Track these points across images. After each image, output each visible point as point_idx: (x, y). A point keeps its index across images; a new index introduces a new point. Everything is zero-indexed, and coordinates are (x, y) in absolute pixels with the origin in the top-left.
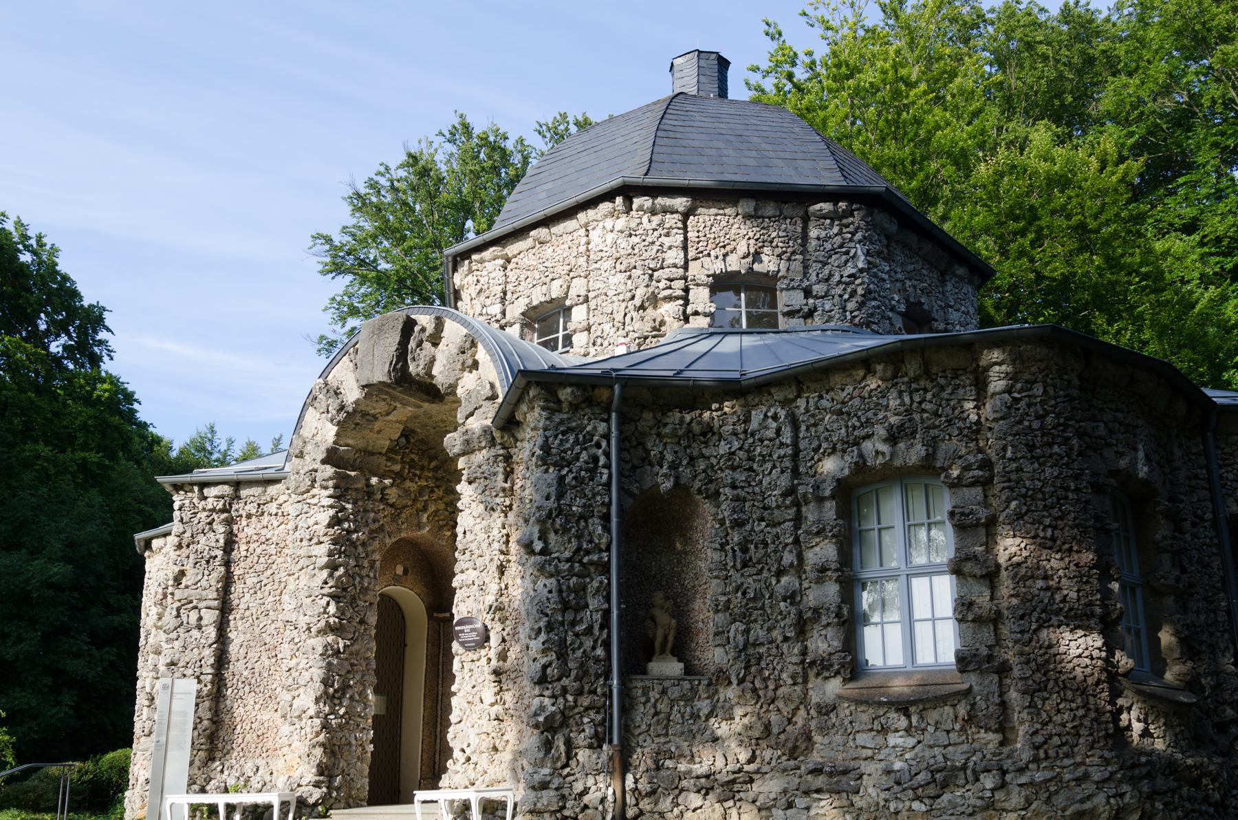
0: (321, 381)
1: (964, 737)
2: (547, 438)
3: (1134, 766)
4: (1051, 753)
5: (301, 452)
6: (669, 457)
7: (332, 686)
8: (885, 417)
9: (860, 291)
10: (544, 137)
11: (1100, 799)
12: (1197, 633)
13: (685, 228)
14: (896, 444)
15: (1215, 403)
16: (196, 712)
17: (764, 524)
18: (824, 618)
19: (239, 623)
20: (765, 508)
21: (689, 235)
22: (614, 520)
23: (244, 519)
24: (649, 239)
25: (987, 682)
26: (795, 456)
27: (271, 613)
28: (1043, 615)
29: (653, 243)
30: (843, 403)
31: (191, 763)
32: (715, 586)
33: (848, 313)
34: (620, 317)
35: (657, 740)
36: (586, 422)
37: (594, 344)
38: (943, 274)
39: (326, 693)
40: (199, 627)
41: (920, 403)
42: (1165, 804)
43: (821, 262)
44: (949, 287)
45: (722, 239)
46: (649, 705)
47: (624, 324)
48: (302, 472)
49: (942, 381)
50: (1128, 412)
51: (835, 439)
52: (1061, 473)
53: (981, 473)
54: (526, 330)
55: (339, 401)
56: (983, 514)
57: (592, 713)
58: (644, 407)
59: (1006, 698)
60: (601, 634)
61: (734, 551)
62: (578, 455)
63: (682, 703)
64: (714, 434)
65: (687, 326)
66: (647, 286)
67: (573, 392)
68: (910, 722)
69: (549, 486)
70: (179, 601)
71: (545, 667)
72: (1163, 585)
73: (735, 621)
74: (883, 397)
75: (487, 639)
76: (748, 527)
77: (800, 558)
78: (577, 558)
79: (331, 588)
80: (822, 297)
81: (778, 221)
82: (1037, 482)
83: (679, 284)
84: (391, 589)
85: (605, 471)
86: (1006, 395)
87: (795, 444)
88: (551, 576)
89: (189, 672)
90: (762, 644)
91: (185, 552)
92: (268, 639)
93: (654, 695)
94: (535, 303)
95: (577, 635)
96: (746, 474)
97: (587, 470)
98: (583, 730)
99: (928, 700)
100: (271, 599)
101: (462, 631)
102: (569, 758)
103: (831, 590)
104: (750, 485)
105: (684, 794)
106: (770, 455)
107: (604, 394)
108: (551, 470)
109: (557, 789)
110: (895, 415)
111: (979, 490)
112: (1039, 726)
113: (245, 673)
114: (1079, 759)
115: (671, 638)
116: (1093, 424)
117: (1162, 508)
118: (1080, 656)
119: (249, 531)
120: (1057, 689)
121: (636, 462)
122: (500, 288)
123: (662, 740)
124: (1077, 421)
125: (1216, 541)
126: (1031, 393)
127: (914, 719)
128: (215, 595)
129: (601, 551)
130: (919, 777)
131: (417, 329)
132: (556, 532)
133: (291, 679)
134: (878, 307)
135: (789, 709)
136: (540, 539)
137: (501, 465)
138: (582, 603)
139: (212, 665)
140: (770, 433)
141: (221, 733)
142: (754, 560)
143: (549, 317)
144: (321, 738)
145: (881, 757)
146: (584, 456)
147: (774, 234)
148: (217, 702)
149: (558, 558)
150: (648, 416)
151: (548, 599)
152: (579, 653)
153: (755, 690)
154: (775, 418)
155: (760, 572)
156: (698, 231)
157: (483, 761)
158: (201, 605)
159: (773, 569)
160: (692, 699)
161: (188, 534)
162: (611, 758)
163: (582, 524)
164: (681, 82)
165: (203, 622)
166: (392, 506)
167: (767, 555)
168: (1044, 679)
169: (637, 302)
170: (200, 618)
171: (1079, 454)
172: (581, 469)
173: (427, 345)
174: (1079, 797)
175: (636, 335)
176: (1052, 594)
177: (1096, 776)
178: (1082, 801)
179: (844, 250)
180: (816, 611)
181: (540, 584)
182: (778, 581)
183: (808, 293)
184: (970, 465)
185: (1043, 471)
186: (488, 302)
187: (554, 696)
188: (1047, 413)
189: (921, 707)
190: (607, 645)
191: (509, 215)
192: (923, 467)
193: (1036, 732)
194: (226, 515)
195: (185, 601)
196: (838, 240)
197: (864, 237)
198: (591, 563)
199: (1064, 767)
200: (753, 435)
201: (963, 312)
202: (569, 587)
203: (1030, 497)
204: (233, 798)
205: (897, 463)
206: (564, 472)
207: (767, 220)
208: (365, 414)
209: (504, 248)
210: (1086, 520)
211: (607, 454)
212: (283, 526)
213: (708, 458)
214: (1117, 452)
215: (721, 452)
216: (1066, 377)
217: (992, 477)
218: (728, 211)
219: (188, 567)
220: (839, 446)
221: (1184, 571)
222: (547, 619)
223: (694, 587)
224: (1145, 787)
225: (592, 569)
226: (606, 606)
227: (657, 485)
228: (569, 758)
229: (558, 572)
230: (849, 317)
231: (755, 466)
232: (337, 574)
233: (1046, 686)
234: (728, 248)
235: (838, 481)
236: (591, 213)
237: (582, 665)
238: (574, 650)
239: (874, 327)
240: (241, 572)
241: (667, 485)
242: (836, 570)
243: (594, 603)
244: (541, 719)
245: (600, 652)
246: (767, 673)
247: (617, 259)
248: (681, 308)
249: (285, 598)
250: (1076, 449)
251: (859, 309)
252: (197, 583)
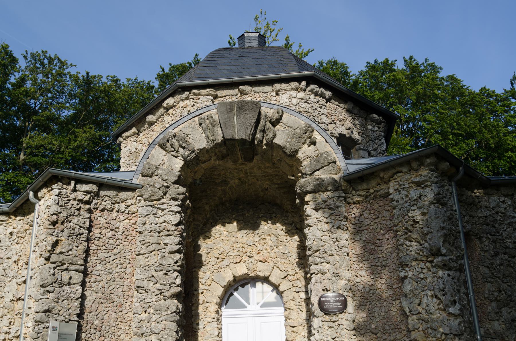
10: (26, 59)
19: (93, 285)
70: (54, 263)
79: (178, 266)
92: (116, 299)
113: (96, 322)
195: (60, 264)
212: (127, 221)
218: (341, 105)
236: (284, 86)
240: (95, 248)
252: (68, 252)
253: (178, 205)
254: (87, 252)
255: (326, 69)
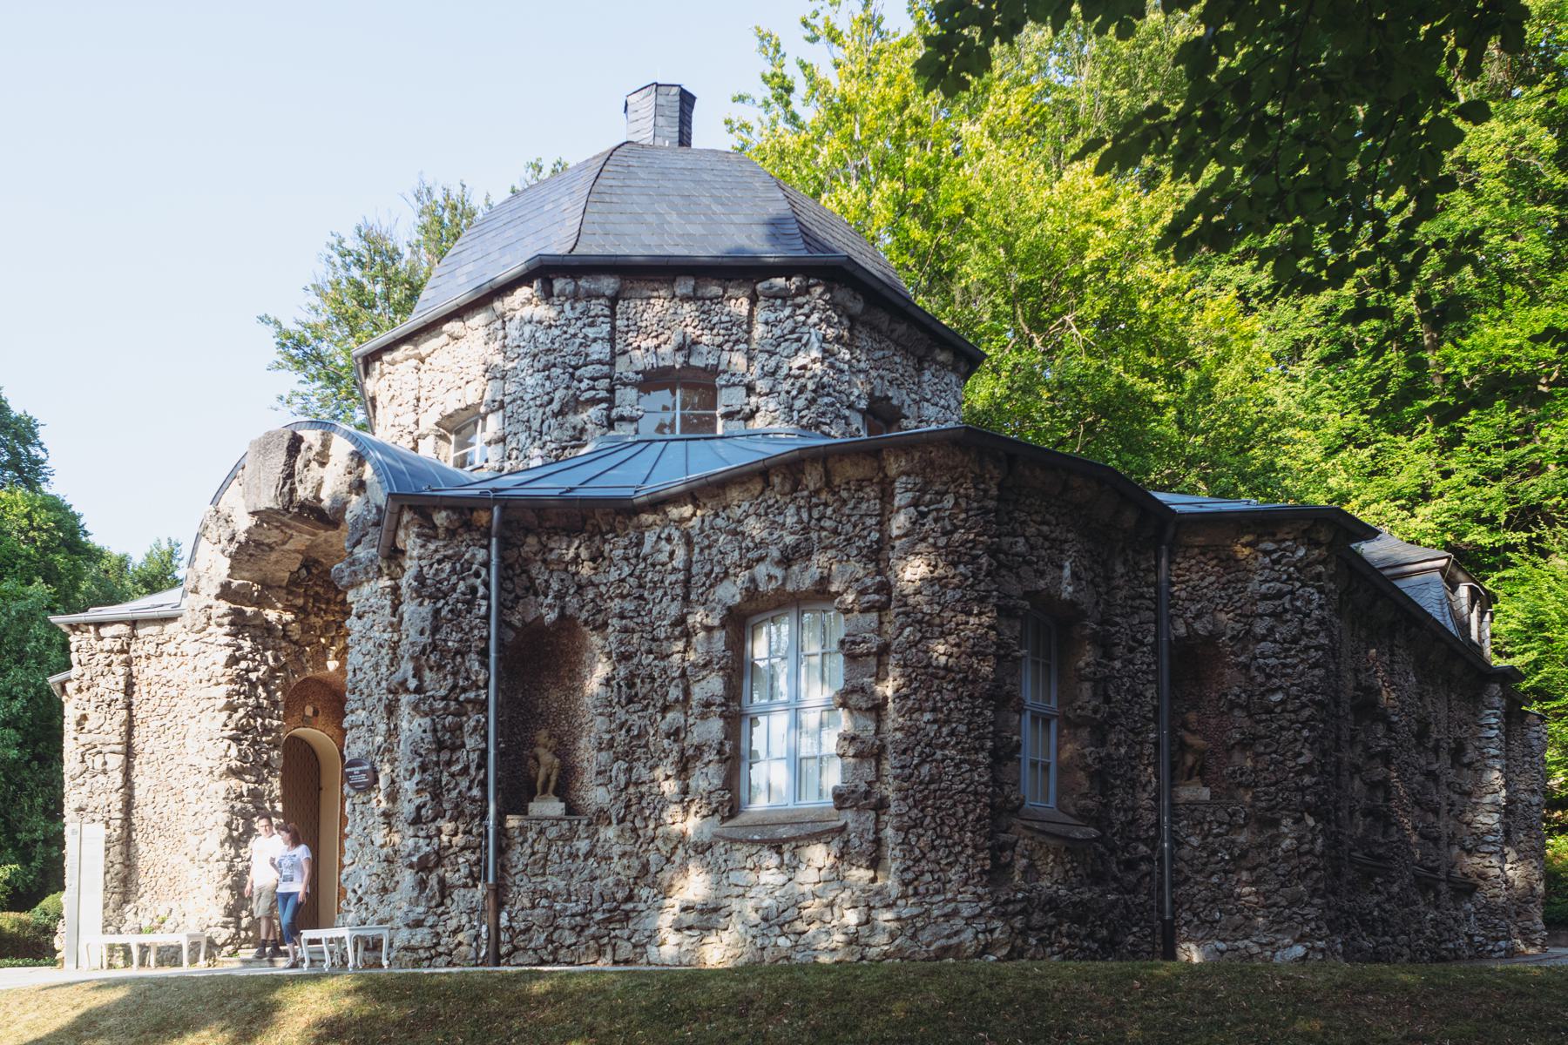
0: (212, 508)
1: (834, 875)
2: (421, 567)
3: (1007, 902)
4: (922, 890)
5: (196, 587)
6: (555, 586)
7: (237, 830)
8: (781, 536)
9: (811, 386)
11: (968, 935)
12: (1114, 766)
13: (613, 315)
14: (790, 566)
15: (1173, 511)
16: (107, 856)
17: (652, 656)
18: (706, 755)
20: (654, 639)
21: (618, 323)
22: (493, 655)
23: (143, 659)
24: (571, 331)
25: (863, 819)
26: (687, 583)
27: (176, 757)
28: (927, 750)
29: (575, 335)
30: (740, 521)
31: (106, 906)
32: (600, 723)
33: (795, 413)
34: (536, 425)
35: (533, 879)
36: (464, 549)
37: (509, 458)
38: (920, 361)
39: (230, 836)
40: (105, 772)
41: (819, 520)
42: (1040, 941)
43: (768, 352)
44: (927, 375)
45: (655, 327)
46: (526, 845)
47: (541, 433)
48: (198, 608)
49: (844, 494)
50: (1057, 525)
51: (728, 562)
52: (964, 596)
53: (877, 597)
54: (441, 443)
55: (230, 530)
56: (874, 643)
57: (467, 854)
58: (528, 531)
59: (882, 835)
60: (477, 775)
61: (620, 686)
62: (455, 585)
63: (560, 843)
64: (604, 559)
65: (612, 433)
66: (568, 388)
67: (448, 517)
68: (782, 860)
69: (424, 619)
71: (419, 808)
72: (1079, 716)
73: (617, 759)
74: (780, 514)
75: (376, 780)
76: (635, 661)
77: (687, 693)
78: (453, 696)
80: (767, 395)
81: (721, 303)
82: (936, 607)
83: (604, 383)
84: (301, 731)
85: (484, 603)
86: (912, 509)
87: (688, 569)
88: (426, 715)
89: (98, 817)
90: (644, 783)
91: (85, 695)
93: (531, 835)
94: (450, 411)
95: (453, 775)
96: (635, 602)
97: (464, 602)
98: (458, 870)
99: (801, 838)
100: (175, 742)
101: (352, 773)
102: (443, 897)
103: (714, 728)
104: (639, 615)
105: (558, 932)
106: (662, 582)
107: (482, 517)
108: (426, 603)
109: (431, 927)
110: (792, 533)
111: (874, 615)
112: (910, 863)
114: (949, 895)
115: (553, 778)
116: (1011, 540)
117: (1088, 631)
118: (963, 791)
119: (150, 673)
120: (933, 825)
121: (520, 592)
122: (413, 394)
123: (540, 879)
124: (990, 537)
125: (1154, 667)
126: (940, 506)
127: (786, 857)
128: (118, 739)
129: (478, 688)
130: (786, 914)
131: (303, 446)
132: (431, 669)
133: (197, 823)
134: (833, 404)
135: (668, 848)
136: (414, 676)
137: (388, 597)
138: (458, 742)
139: (120, 810)
140: (664, 557)
141: (134, 877)
142: (640, 696)
143: (464, 428)
144: (228, 881)
145: (752, 894)
146: (461, 586)
147: (716, 319)
148: (128, 846)
149: (433, 696)
150: (532, 540)
151: (422, 739)
152: (454, 794)
153: (634, 830)
154: (669, 539)
155: (645, 708)
156: (628, 319)
157: (373, 900)
158: (106, 749)
159: (659, 705)
160: (571, 839)
161: (87, 677)
162: (485, 897)
163: (459, 659)
164: (636, 126)
165: (108, 767)
166: (296, 643)
167: (652, 689)
168: (920, 815)
169: (555, 406)
170: (105, 763)
171: (988, 574)
172: (458, 601)
173: (314, 465)
174: (946, 933)
175: (553, 446)
176: (940, 728)
177: (966, 911)
178: (949, 937)
179: (795, 336)
180: (699, 749)
181: (415, 723)
182: (663, 718)
183: (750, 389)
184: (866, 588)
185: (944, 594)
186: (400, 410)
187: (428, 837)
188: (956, 528)
189: (794, 844)
190: (483, 784)
191: (427, 305)
192: (817, 592)
193: (907, 869)
194: (125, 656)
196: (789, 324)
197: (821, 320)
198: (468, 701)
199: (932, 904)
200: (645, 559)
201: (943, 407)
202: (444, 726)
203: (928, 622)
204: (146, 939)
205: (790, 587)
206: (440, 605)
207: (708, 302)
208: (258, 544)
209: (416, 346)
210: (987, 647)
211: (487, 585)
212: (183, 667)
213: (597, 586)
214: (1036, 571)
215: (611, 579)
216: (982, 486)
217: (890, 600)
218: (662, 293)
219: (90, 711)
220: (731, 571)
221: (1107, 700)
222: (420, 759)
223: (581, 725)
224: (1018, 923)
225: (469, 707)
226: (483, 745)
227: (541, 617)
228: (443, 897)
229: (433, 711)
230: (796, 418)
231: (646, 594)
232: (236, 716)
233: (922, 823)
234: (662, 338)
235: (729, 609)
237: (457, 805)
238: (449, 791)
239: (826, 428)
240: (144, 715)
241: (551, 616)
242: (721, 705)
243: (470, 742)
244: (415, 859)
245: (476, 792)
246: (647, 812)
247: (535, 356)
248: (605, 413)
249: (188, 741)
250: (984, 568)
251: (808, 408)
253: (227, 635)
254: (130, 725)
255: (920, 361)
